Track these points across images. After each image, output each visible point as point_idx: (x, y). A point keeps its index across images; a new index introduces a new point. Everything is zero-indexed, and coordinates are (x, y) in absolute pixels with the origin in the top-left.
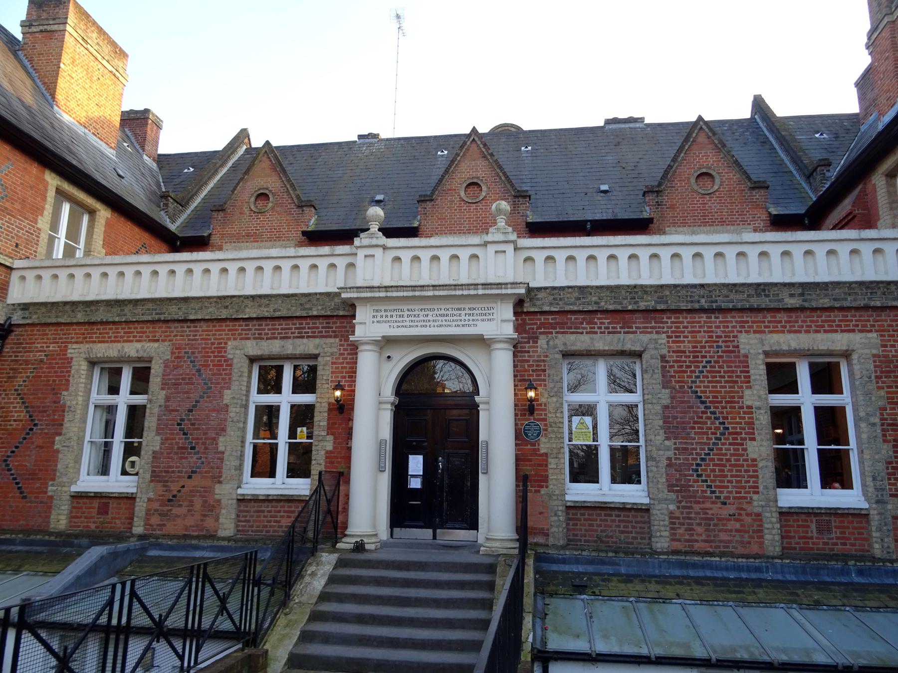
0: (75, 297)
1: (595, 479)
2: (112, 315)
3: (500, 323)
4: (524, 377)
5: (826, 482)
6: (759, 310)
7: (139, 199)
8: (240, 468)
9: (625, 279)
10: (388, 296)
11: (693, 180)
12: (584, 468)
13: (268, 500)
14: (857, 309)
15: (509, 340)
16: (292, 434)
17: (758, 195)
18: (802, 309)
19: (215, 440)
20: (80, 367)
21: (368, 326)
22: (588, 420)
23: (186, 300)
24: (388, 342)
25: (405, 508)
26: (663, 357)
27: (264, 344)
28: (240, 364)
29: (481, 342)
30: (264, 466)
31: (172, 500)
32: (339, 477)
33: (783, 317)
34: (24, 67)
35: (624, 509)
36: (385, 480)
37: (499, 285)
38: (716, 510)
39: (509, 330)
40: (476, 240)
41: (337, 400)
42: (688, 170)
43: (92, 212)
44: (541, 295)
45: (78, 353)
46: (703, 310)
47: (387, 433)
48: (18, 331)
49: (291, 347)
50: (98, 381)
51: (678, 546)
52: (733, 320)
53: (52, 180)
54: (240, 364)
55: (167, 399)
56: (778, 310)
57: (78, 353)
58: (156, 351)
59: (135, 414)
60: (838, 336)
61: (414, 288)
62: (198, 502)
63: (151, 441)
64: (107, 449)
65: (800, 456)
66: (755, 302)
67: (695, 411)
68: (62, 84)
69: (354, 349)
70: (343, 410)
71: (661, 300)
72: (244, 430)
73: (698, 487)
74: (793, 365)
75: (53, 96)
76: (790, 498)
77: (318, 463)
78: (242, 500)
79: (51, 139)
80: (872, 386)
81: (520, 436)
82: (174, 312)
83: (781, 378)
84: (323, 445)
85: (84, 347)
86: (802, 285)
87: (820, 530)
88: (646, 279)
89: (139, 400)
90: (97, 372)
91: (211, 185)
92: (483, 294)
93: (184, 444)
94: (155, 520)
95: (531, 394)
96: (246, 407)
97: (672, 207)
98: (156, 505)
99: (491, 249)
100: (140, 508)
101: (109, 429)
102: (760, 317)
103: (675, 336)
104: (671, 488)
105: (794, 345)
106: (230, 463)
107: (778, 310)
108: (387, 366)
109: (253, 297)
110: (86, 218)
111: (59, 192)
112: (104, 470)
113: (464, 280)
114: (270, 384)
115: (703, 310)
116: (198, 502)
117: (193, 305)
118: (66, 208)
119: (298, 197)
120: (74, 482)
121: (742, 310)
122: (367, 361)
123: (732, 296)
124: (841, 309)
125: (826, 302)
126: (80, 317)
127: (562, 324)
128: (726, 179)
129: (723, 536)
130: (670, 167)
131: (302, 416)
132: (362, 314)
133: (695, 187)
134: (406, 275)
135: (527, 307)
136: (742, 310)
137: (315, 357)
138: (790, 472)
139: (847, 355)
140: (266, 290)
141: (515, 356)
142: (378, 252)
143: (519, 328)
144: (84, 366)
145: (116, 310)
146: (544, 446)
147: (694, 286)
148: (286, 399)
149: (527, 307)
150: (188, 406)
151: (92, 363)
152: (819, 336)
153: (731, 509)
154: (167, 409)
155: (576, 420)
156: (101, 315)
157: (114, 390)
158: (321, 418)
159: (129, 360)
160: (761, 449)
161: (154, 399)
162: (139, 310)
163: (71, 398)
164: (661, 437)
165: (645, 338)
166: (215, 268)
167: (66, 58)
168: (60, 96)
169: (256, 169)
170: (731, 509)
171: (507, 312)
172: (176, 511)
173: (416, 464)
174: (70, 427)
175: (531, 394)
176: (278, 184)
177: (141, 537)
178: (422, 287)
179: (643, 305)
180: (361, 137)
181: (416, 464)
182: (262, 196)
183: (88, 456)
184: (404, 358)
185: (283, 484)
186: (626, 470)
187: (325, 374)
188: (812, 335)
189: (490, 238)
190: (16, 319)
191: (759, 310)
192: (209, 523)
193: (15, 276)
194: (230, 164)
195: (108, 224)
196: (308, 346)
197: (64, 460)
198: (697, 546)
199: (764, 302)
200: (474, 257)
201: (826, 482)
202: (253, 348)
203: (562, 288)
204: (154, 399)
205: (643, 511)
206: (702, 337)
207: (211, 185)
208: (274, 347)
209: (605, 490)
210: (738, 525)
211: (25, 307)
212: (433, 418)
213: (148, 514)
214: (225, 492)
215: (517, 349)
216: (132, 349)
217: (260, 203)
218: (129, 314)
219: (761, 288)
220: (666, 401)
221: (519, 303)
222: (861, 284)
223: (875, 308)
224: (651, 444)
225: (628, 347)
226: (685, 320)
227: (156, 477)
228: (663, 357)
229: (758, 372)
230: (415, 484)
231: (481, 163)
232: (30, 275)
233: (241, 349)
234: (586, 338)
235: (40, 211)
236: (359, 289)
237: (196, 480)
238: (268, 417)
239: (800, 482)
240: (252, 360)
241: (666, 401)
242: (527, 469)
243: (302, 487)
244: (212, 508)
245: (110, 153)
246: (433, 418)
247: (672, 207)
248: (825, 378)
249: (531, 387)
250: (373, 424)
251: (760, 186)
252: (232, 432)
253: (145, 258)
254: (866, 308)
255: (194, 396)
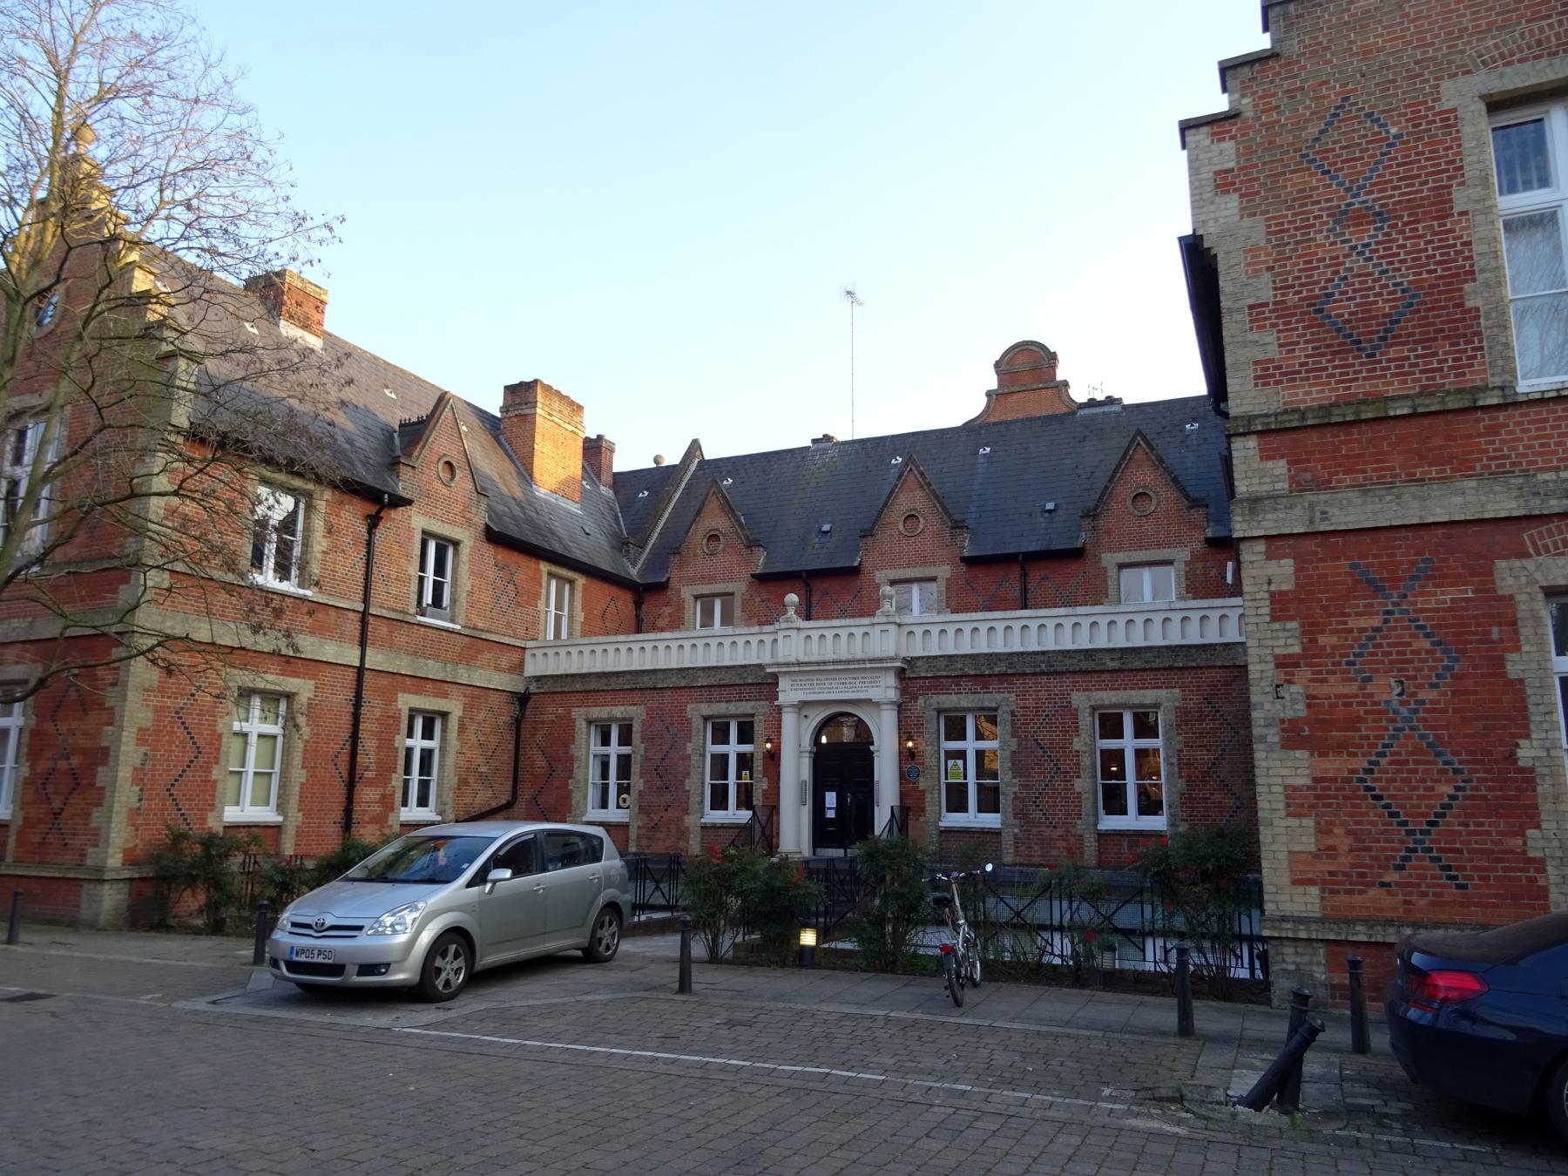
0: (573, 671)
1: (964, 809)
2: (601, 685)
3: (885, 689)
4: (904, 732)
5: (981, 809)
6: (1087, 672)
7: (604, 564)
8: (702, 802)
9: (983, 648)
10: (803, 669)
11: (1129, 502)
12: (957, 800)
13: (723, 827)
14: (1165, 669)
15: (893, 703)
16: (739, 777)
17: (1198, 515)
18: (1121, 670)
19: (682, 783)
20: (581, 725)
21: (788, 693)
22: (960, 762)
23: (654, 671)
24: (803, 705)
25: (823, 832)
26: (1012, 713)
27: (714, 706)
28: (697, 722)
29: (877, 705)
30: (719, 801)
31: (655, 827)
32: (773, 809)
33: (1106, 677)
34: (505, 451)
35: (983, 832)
36: (806, 813)
37: (881, 660)
38: (1048, 832)
39: (892, 695)
40: (866, 621)
41: (769, 751)
42: (1125, 491)
43: (571, 582)
44: (919, 663)
45: (579, 714)
46: (1042, 673)
47: (806, 774)
48: (534, 698)
49: (733, 708)
50: (594, 737)
51: (1019, 860)
52: (1067, 680)
53: (544, 567)
54: (697, 722)
55: (646, 750)
56: (1103, 672)
57: (579, 714)
58: (635, 712)
59: (624, 761)
60: (1149, 692)
61: (818, 663)
62: (673, 828)
63: (637, 782)
64: (605, 790)
65: (1122, 790)
66: (1084, 665)
67: (1040, 755)
68: (537, 462)
69: (779, 709)
70: (773, 757)
71: (1011, 665)
72: (703, 774)
73: (1036, 815)
74: (1121, 715)
75: (531, 475)
76: (1111, 823)
77: (757, 800)
78: (704, 827)
79: (536, 528)
80: (1173, 733)
81: (903, 776)
82: (646, 682)
83: (1111, 726)
84: (760, 785)
85: (583, 710)
86: (1122, 650)
87: (1130, 847)
88: (1000, 648)
89: (626, 750)
90: (593, 729)
91: (666, 515)
92: (869, 666)
93: (656, 779)
94: (644, 842)
95: (910, 744)
96: (704, 756)
97: (1108, 532)
98: (644, 831)
99: (878, 629)
100: (633, 832)
101: (605, 774)
102: (1088, 678)
103: (1022, 695)
104: (1016, 816)
105: (1114, 700)
106: (694, 799)
107: (1103, 672)
108: (805, 723)
109: (704, 669)
110: (567, 587)
111: (551, 575)
112: (604, 805)
113: (859, 655)
114: (721, 736)
115: (1042, 673)
116: (673, 828)
117: (660, 676)
118: (554, 583)
119: (747, 537)
120: (584, 814)
121: (1074, 672)
122: (788, 719)
123: (1067, 661)
124: (1152, 669)
125: (1138, 664)
126: (578, 687)
127: (936, 687)
128: (1165, 497)
129: (1054, 853)
130: (1106, 488)
131: (744, 761)
132: (783, 684)
133: (1131, 509)
134: (815, 652)
135: (909, 674)
136: (1074, 672)
137: (752, 715)
138: (1115, 803)
139: (1157, 706)
140: (713, 663)
141: (899, 713)
142: (794, 633)
143: (903, 691)
144: (584, 725)
145: (604, 681)
146: (922, 785)
147: (1037, 653)
148: (733, 748)
149: (909, 674)
150: (661, 755)
151: (589, 722)
152: (1134, 692)
153: (1060, 832)
154: (646, 758)
155: (950, 762)
156: (593, 685)
157: (606, 741)
158: (758, 765)
159: (616, 720)
160: (1087, 785)
161: (636, 749)
162: (621, 680)
163: (577, 750)
164: (1009, 776)
165: (999, 697)
166: (674, 645)
167: (538, 439)
168: (537, 475)
169: (706, 510)
170: (1060, 832)
171: (891, 680)
172: (658, 835)
173: (831, 799)
174: (578, 773)
175: (910, 744)
176: (728, 525)
177: (635, 854)
178: (825, 663)
179: (997, 670)
180: (814, 441)
181: (831, 799)
182: (713, 537)
183: (592, 795)
184: (818, 716)
185: (736, 815)
186: (989, 801)
187: (760, 729)
188: (1129, 692)
189: (876, 620)
190: (533, 689)
191: (1087, 672)
192: (682, 844)
193: (528, 654)
194: (683, 485)
195: (584, 590)
196: (746, 707)
197: (576, 797)
198: (1034, 860)
199: (1090, 665)
200: (866, 634)
201: (981, 809)
202: (706, 709)
203: (935, 657)
204: (636, 749)
205: (996, 833)
206: (1043, 695)
207: (666, 515)
208: (720, 708)
209: (973, 818)
210: (1064, 844)
211: (538, 679)
212: (842, 762)
213: (639, 837)
214: (691, 821)
215: (900, 708)
216: (618, 711)
217: (713, 544)
218: (614, 683)
219: (1089, 654)
220: (1014, 748)
221: (901, 673)
222: (1168, 648)
223: (1179, 668)
224: (1008, 783)
225: (986, 704)
226: (1030, 681)
227: (642, 810)
228: (1012, 713)
229: (1087, 722)
230: (831, 814)
231: (919, 493)
232: (539, 653)
233: (697, 710)
234: (954, 698)
235: (537, 596)
236: (779, 665)
237: (671, 813)
238: (720, 762)
239: (963, 808)
240: (706, 719)
241: (1014, 748)
242: (909, 802)
243: (744, 816)
244: (683, 833)
245: (575, 509)
246: (842, 762)
247: (1108, 532)
248: (1145, 728)
249: (910, 739)
250: (795, 770)
251: (1196, 503)
252: (694, 776)
253: (622, 638)
254: (1171, 668)
255: (666, 748)
